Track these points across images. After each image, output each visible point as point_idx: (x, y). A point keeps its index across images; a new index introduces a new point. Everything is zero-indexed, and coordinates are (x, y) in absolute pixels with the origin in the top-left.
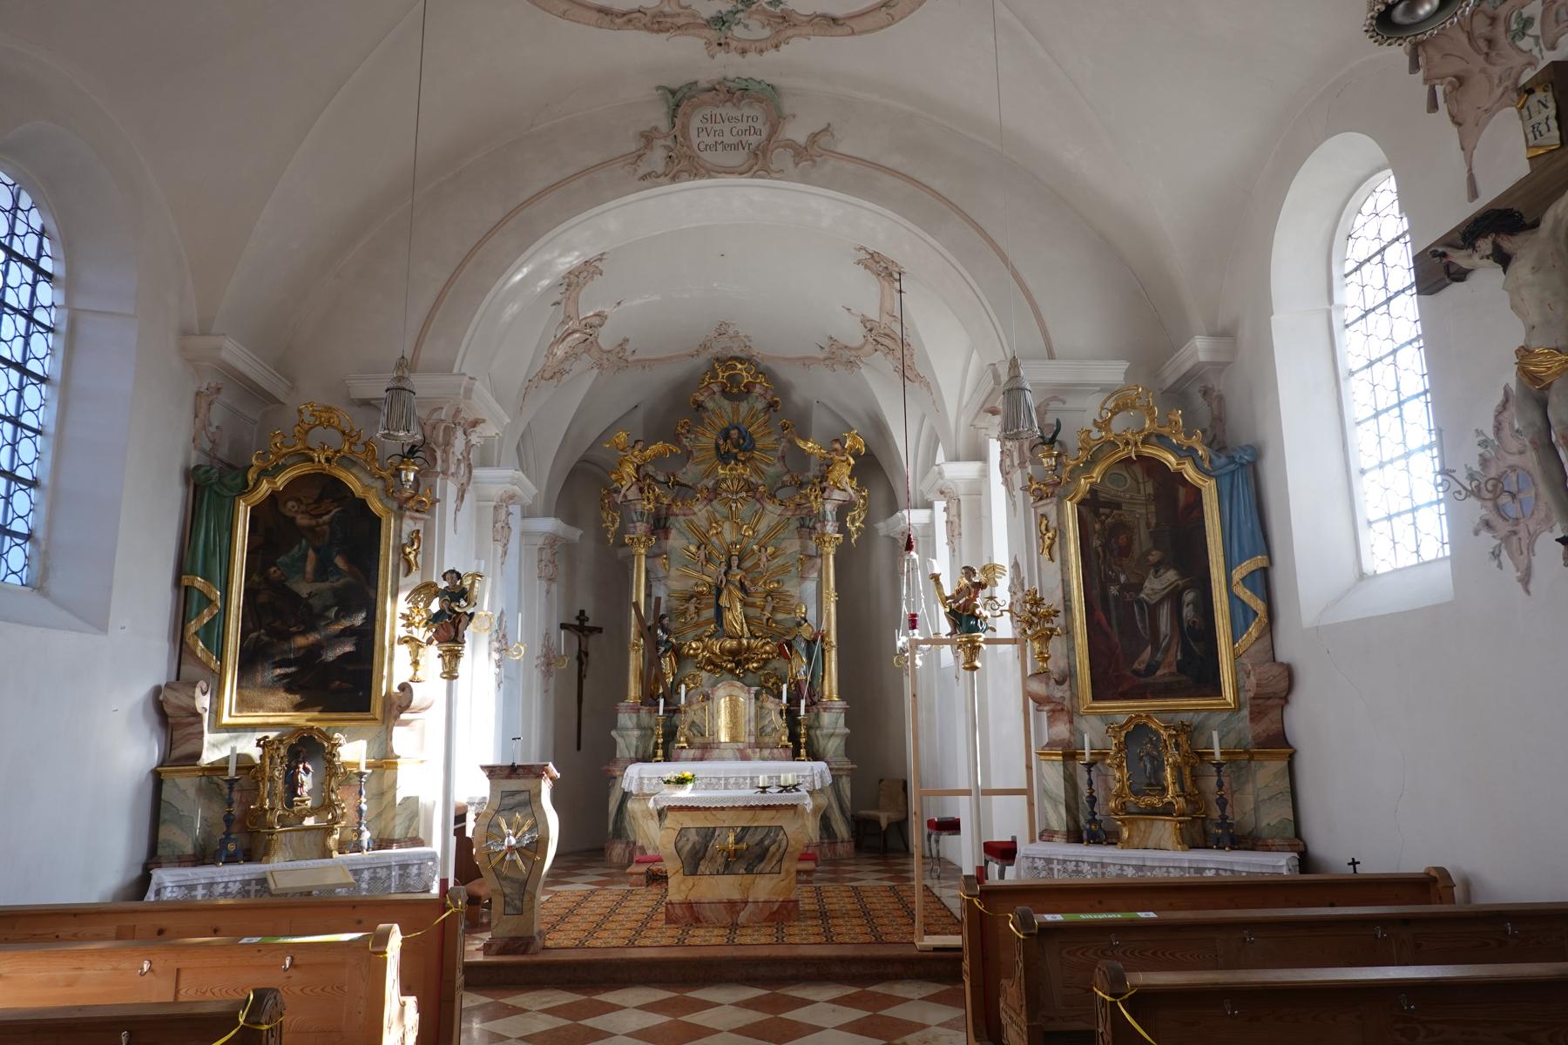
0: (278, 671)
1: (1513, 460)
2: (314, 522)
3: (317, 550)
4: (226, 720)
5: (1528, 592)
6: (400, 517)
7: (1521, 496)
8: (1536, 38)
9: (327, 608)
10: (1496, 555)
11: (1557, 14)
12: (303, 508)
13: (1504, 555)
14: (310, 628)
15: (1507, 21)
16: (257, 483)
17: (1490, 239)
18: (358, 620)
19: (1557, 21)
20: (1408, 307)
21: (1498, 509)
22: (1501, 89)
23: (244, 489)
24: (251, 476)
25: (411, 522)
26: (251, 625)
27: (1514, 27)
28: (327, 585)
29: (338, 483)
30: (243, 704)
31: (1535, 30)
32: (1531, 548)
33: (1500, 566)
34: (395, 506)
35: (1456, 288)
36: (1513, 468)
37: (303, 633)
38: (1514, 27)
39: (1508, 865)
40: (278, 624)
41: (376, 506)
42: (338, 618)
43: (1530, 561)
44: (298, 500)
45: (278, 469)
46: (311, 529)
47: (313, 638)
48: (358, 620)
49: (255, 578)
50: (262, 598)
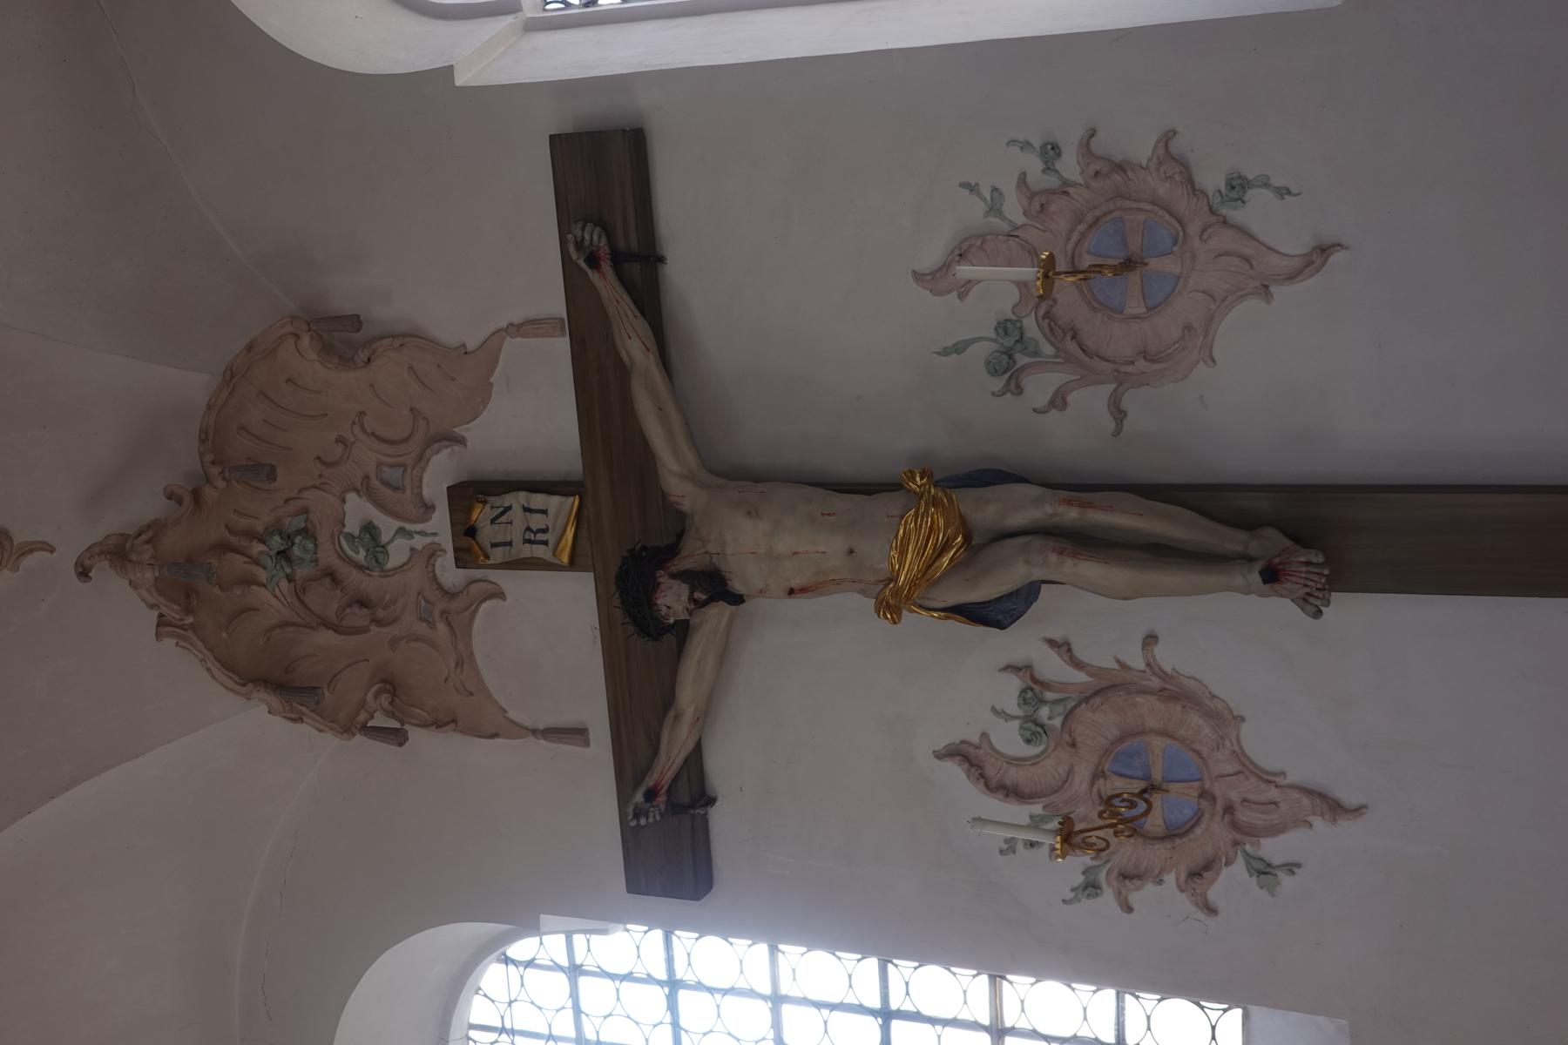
1: (1083, 774)
5: (1359, 810)
7: (1157, 775)
8: (401, 531)
10: (1264, 871)
11: (385, 483)
13: (1272, 849)
15: (345, 558)
17: (664, 580)
19: (395, 489)
20: (714, 955)
21: (1172, 834)
22: (441, 627)
27: (361, 556)
31: (387, 526)
32: (1268, 778)
33: (1291, 868)
35: (722, 819)
36: (1098, 774)
38: (361, 556)
43: (1293, 787)
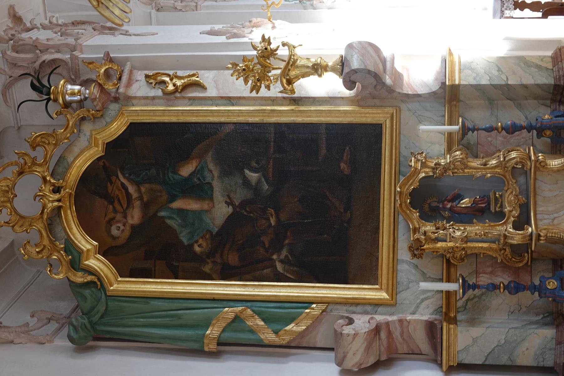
2: (137, 203)
3: (173, 198)
6: (129, 99)
9: (246, 182)
12: (119, 217)
16: (90, 271)
24: (79, 278)
25: (135, 87)
29: (86, 178)
34: (114, 107)
40: (266, 240)
44: (110, 223)
45: (70, 247)
46: (145, 206)
49: (207, 268)
50: (233, 259)
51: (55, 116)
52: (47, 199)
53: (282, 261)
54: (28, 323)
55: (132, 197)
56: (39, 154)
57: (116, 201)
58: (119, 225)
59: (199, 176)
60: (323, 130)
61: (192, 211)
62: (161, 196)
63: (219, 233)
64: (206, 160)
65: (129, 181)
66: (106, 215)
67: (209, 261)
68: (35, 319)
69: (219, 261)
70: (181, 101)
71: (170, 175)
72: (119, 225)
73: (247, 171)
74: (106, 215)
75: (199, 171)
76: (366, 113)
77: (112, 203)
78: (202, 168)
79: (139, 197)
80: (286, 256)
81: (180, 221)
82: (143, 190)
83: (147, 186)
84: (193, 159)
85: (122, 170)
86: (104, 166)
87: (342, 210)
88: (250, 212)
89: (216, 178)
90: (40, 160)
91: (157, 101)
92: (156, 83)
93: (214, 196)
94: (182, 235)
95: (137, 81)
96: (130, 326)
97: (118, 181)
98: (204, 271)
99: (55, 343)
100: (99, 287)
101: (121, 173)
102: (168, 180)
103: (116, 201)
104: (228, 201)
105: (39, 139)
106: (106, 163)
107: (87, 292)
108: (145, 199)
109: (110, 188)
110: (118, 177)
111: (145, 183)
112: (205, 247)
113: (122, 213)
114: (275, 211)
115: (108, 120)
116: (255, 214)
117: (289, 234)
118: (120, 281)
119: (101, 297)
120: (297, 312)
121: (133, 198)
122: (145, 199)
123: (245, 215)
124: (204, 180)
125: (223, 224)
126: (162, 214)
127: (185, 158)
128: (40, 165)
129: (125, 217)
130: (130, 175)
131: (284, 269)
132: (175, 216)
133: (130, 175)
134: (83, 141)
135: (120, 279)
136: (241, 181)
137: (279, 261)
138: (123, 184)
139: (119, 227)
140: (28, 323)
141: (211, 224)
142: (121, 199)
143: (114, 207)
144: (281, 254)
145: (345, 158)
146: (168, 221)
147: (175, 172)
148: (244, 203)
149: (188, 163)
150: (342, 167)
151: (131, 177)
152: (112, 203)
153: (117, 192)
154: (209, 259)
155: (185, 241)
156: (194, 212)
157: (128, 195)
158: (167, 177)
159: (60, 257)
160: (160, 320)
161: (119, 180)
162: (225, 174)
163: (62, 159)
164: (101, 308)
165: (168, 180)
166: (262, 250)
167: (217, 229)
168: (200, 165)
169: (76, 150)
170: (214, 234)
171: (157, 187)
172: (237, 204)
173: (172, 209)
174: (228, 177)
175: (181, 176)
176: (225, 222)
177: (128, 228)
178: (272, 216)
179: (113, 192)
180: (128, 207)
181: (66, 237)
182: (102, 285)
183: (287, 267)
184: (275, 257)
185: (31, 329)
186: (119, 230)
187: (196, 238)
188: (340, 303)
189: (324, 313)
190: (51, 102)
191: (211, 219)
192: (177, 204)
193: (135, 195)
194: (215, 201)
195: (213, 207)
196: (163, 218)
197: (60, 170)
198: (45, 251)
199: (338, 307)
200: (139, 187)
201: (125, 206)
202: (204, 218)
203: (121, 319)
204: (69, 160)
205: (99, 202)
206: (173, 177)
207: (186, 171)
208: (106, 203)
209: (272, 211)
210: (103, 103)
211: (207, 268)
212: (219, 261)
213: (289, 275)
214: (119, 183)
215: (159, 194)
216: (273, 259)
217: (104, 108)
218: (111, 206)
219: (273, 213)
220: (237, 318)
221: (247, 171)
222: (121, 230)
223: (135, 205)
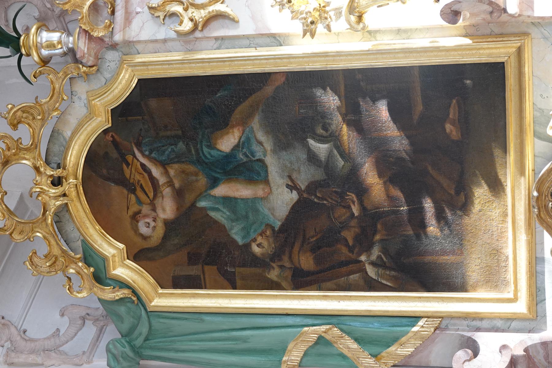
0: (433, 228)
2: (167, 191)
3: (215, 183)
4: (521, 307)
6: (129, 47)
9: (312, 158)
12: (146, 209)
14: (353, 181)
16: (122, 284)
18: (331, 100)
23: (137, 299)
24: (110, 294)
25: (136, 23)
26: (354, 277)
28: (269, 160)
29: (92, 160)
30: (493, 277)
34: (111, 56)
37: (362, 191)
39: (551, 16)
40: (349, 235)
41: (124, 84)
42: (333, 138)
44: (135, 217)
45: (90, 256)
46: (179, 194)
47: (370, 176)
48: (331, 100)
49: (274, 275)
50: (306, 262)
51: (32, 79)
52: (46, 195)
53: (373, 264)
54: (58, 329)
55: (158, 183)
56: (24, 134)
57: (138, 189)
58: (147, 220)
59: (244, 150)
60: (416, 73)
61: (242, 199)
62: (197, 181)
63: (284, 228)
64: (252, 128)
65: (151, 161)
66: (128, 208)
67: (274, 265)
68: (66, 318)
69: (287, 264)
70: (204, 43)
71: (205, 150)
72: (147, 220)
73: (311, 142)
74: (128, 208)
75: (244, 143)
76: (479, 49)
77: (134, 191)
78: (248, 139)
79: (168, 182)
80: (379, 257)
81: (228, 213)
82: (172, 172)
83: (176, 166)
84: (233, 127)
85: (139, 145)
86: (115, 143)
87: (453, 192)
88: (323, 199)
89: (269, 152)
90: (27, 142)
91: (170, 44)
92: (165, 16)
93: (270, 178)
94: (233, 231)
95: (137, 13)
96: (184, 351)
97: (135, 161)
98: (268, 278)
99: (95, 363)
100: (136, 302)
101: (138, 149)
102: (203, 158)
103: (138, 189)
104: (290, 183)
105: (19, 113)
106: (116, 137)
107: (122, 310)
108: (177, 185)
109: (127, 171)
110: (134, 156)
111: (174, 163)
112: (266, 247)
113: (149, 204)
114: (357, 196)
115: (108, 76)
116: (330, 200)
117: (379, 226)
118: (161, 293)
119: (141, 315)
120: (401, 331)
121: (161, 183)
122: (177, 185)
123: (315, 203)
124: (254, 157)
125: (287, 216)
126: (202, 204)
127: (223, 124)
128: (27, 150)
129: (154, 210)
130: (151, 153)
131: (378, 274)
132: (220, 207)
133: (151, 153)
134: (78, 110)
135: (161, 291)
136: (305, 156)
137: (369, 264)
138: (143, 165)
139: (149, 224)
140: (58, 329)
141: (271, 216)
142: (144, 185)
143: (137, 198)
144: (371, 254)
145: (451, 116)
146: (212, 214)
147: (212, 146)
148: (313, 187)
149: (227, 133)
150: (448, 130)
151: (153, 155)
152: (134, 191)
153: (138, 177)
154: (274, 262)
155: (240, 242)
156: (245, 200)
157: (153, 179)
158: (201, 154)
159: (78, 269)
160: (220, 343)
161: (138, 160)
162: (282, 146)
163: (55, 134)
164: (144, 329)
165: (203, 158)
166: (344, 250)
167: (279, 223)
168: (245, 135)
169: (73, 121)
170: (276, 229)
171: (191, 168)
172: (303, 187)
173: (215, 197)
174: (286, 151)
175: (221, 151)
176: (290, 212)
177: (160, 224)
178: (354, 203)
179: (132, 177)
180: (155, 196)
181: (82, 238)
182: (139, 298)
183: (381, 271)
184: (363, 258)
185: (63, 339)
186: (148, 227)
187: (253, 236)
188: (459, 318)
189: (437, 332)
190: (23, 57)
191: (269, 209)
192: (221, 190)
193: (162, 180)
194: (272, 185)
195: (271, 192)
196: (204, 209)
197: (56, 148)
198: (57, 263)
199: (457, 322)
200: (165, 169)
201: (151, 195)
202: (261, 209)
203: (171, 342)
204: (65, 134)
205: (116, 190)
206: (209, 153)
207: (227, 143)
208: (125, 192)
209: (353, 195)
210: (95, 54)
211: (274, 275)
212: (287, 264)
213: (384, 282)
214: (138, 164)
215: (194, 178)
216: (361, 261)
217: (98, 58)
218: (132, 195)
219: (355, 199)
220: (321, 340)
221: (311, 142)
222: (151, 227)
223: (164, 193)
